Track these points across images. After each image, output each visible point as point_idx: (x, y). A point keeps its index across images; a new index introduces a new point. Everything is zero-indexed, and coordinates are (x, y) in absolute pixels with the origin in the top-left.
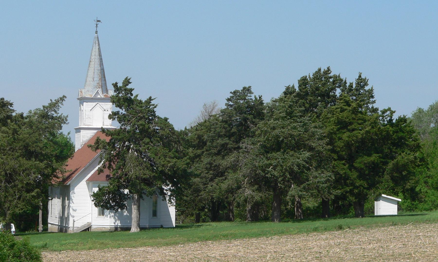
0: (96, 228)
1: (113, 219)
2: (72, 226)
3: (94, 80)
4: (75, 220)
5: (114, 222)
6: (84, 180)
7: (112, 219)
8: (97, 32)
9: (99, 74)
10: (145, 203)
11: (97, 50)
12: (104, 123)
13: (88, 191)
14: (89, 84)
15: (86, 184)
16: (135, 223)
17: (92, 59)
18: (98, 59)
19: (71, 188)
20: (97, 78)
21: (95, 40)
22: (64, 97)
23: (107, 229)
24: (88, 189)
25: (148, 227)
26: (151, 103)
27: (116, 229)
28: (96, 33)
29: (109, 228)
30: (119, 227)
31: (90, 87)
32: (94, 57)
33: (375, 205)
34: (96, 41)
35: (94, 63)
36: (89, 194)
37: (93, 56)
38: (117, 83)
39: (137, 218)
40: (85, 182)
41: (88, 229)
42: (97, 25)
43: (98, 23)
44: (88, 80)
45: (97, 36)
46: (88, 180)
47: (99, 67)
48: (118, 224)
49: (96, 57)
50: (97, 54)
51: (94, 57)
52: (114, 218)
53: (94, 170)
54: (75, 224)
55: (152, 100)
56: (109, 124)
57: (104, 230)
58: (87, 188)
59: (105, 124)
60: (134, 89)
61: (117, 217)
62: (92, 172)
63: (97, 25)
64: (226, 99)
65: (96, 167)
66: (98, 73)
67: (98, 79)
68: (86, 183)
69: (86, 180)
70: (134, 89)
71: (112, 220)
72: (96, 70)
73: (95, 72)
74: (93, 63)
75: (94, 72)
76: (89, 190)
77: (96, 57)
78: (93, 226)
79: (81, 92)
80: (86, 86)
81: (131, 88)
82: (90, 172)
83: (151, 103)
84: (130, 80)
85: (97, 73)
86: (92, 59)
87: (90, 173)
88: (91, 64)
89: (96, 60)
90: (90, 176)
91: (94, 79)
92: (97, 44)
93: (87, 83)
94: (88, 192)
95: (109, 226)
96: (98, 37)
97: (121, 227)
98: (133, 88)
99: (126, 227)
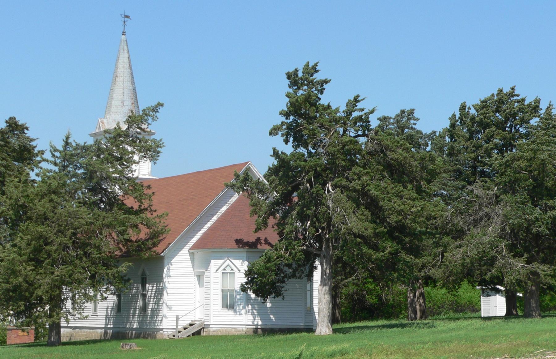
0: (219, 330)
1: (251, 316)
2: (175, 327)
3: (123, 105)
4: (179, 317)
5: (252, 321)
6: (185, 248)
7: (249, 316)
8: (125, 32)
9: (130, 96)
10: (298, 287)
11: (126, 60)
12: (140, 171)
13: (191, 266)
14: (116, 111)
15: (188, 255)
16: (326, 319)
17: (119, 73)
18: (128, 73)
19: (166, 261)
20: (128, 102)
21: (122, 44)
22: (160, 105)
23: (239, 331)
24: (191, 264)
25: (302, 327)
26: (356, 106)
27: (256, 331)
28: (123, 35)
29: (245, 330)
30: (259, 327)
31: (118, 115)
32: (122, 70)
33: (482, 306)
34: (124, 47)
35: (123, 79)
36: (193, 271)
37: (120, 69)
38: (298, 71)
39: (329, 309)
40: (188, 252)
41: (198, 333)
42: (124, 23)
43: (126, 19)
44: (113, 104)
45: (125, 39)
46: (194, 247)
47: (131, 86)
48: (258, 322)
49: (125, 70)
50: (127, 65)
51: (122, 70)
52: (252, 315)
53: (201, 232)
54: (175, 324)
55: (359, 101)
56: (147, 173)
57: (234, 332)
58: (190, 262)
59: (141, 173)
60: (330, 80)
61: (256, 310)
62: (198, 234)
63: (124, 23)
64: (271, 156)
65: (204, 227)
66: (130, 95)
67: (130, 104)
68: (189, 253)
69: (189, 248)
70: (330, 80)
71: (249, 318)
72: (127, 90)
73: (125, 92)
74: (121, 79)
75: (123, 93)
76: (193, 268)
77: (125, 70)
78: (211, 326)
79: (103, 123)
80: (111, 113)
81: (326, 79)
82: (195, 235)
83: (356, 106)
84: (317, 66)
85: (128, 94)
86: (119, 73)
87: (195, 237)
88: (117, 80)
89: (125, 75)
90: (195, 242)
91: (123, 103)
92: (126, 51)
93: (112, 108)
94: (192, 269)
95: (244, 326)
96: (126, 41)
97: (263, 327)
98: (329, 79)
99: (270, 327)
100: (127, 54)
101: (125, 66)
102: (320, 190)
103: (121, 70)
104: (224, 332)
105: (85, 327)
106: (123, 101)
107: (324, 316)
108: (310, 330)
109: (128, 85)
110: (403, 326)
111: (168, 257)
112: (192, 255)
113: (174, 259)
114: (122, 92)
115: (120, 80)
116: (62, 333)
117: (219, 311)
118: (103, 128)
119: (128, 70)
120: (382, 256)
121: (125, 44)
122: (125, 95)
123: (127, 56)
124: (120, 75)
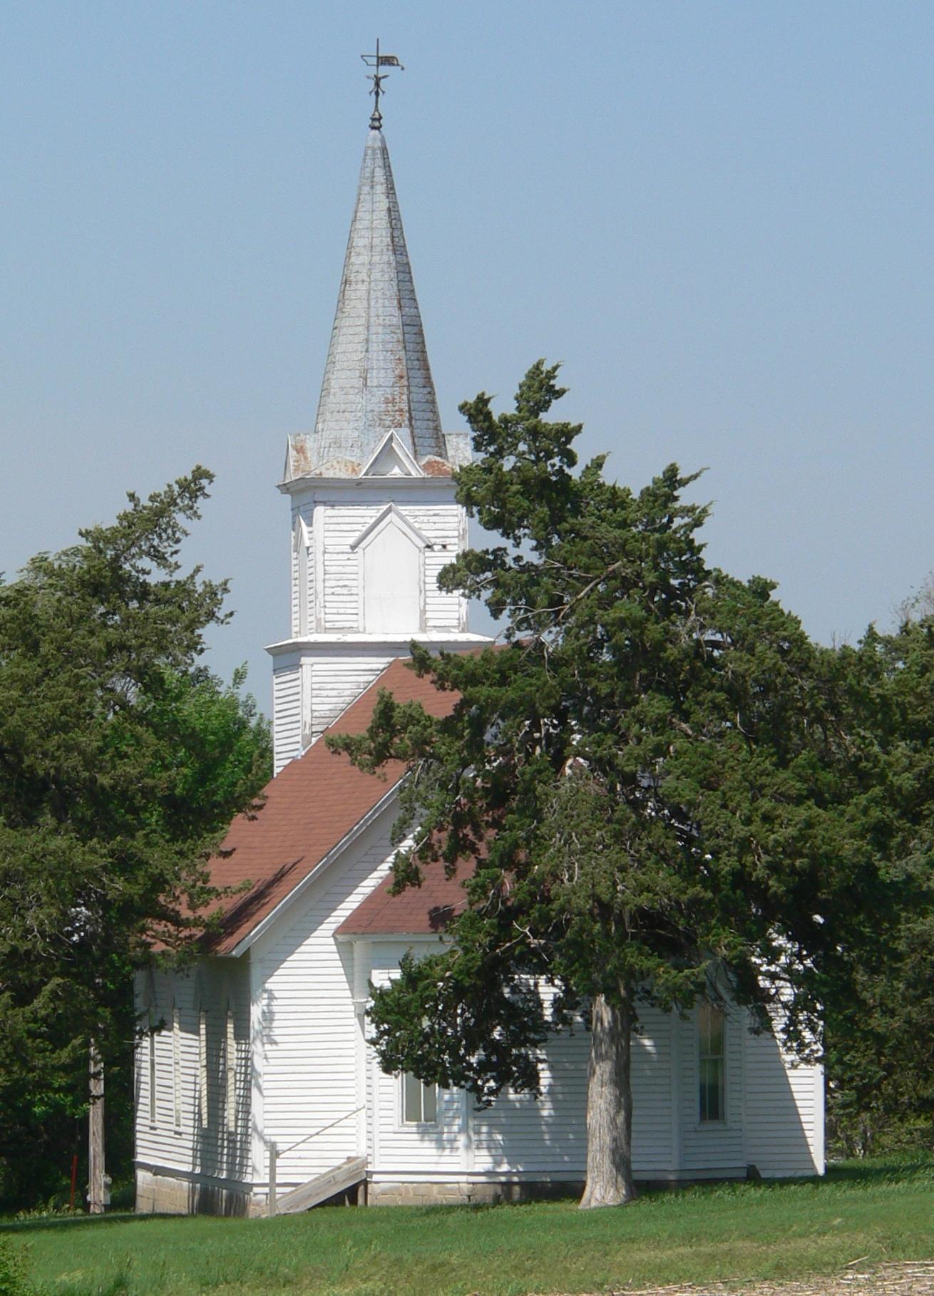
0: (397, 1188)
2: (267, 1181)
3: (365, 385)
4: (280, 1147)
12: (428, 615)
13: (346, 985)
14: (343, 407)
15: (334, 948)
17: (355, 268)
19: (255, 972)
23: (451, 1191)
24: (344, 978)
25: (672, 1177)
28: (373, 128)
29: (465, 1187)
30: (516, 1179)
31: (348, 421)
32: (365, 258)
40: (332, 941)
42: (377, 85)
43: (384, 70)
45: (378, 144)
46: (344, 929)
47: (397, 313)
53: (375, 874)
54: (278, 1170)
55: (684, 483)
56: (455, 623)
57: (437, 1197)
58: (342, 971)
60: (580, 427)
66: (390, 346)
67: (391, 378)
68: (337, 943)
69: (334, 926)
70: (580, 427)
72: (380, 329)
75: (367, 340)
76: (352, 990)
77: (376, 259)
79: (300, 450)
80: (328, 416)
83: (676, 499)
85: (385, 342)
86: (355, 268)
89: (376, 275)
90: (355, 906)
91: (366, 379)
92: (380, 189)
95: (464, 1178)
96: (384, 150)
100: (383, 197)
101: (376, 241)
102: (546, 769)
103: (361, 259)
104: (411, 1195)
105: (178, 1171)
106: (366, 371)
107: (601, 1150)
108: (572, 1190)
109: (386, 311)
110: (65, 1226)
111: (261, 960)
112: (345, 950)
113: (285, 964)
114: (363, 337)
115: (357, 292)
116: (139, 1183)
117: (397, 1129)
118: (297, 469)
119: (385, 258)
120: (687, 977)
121: (379, 162)
122: (374, 347)
123: (383, 204)
124: (360, 277)
